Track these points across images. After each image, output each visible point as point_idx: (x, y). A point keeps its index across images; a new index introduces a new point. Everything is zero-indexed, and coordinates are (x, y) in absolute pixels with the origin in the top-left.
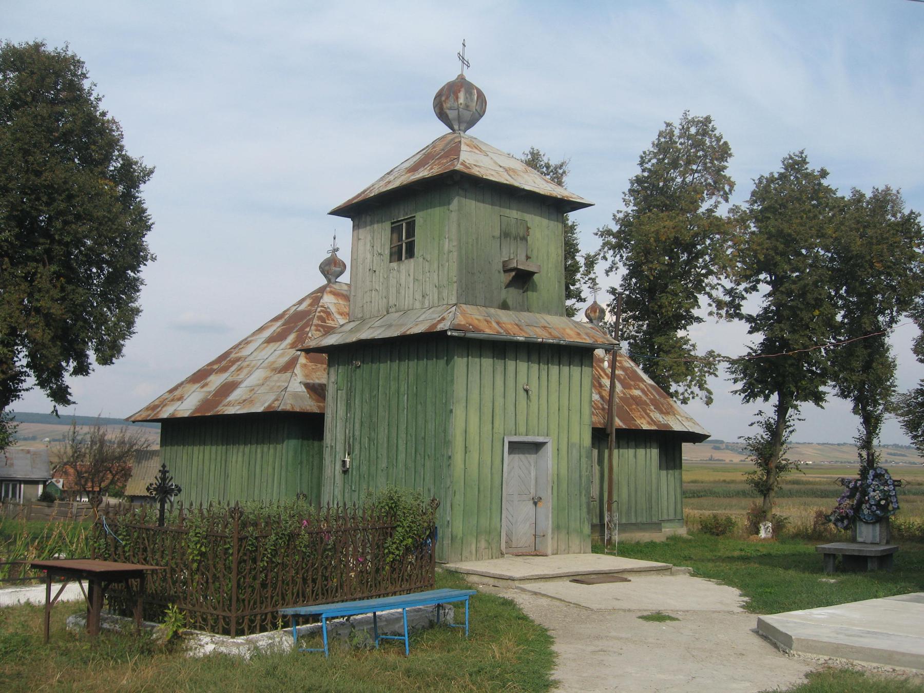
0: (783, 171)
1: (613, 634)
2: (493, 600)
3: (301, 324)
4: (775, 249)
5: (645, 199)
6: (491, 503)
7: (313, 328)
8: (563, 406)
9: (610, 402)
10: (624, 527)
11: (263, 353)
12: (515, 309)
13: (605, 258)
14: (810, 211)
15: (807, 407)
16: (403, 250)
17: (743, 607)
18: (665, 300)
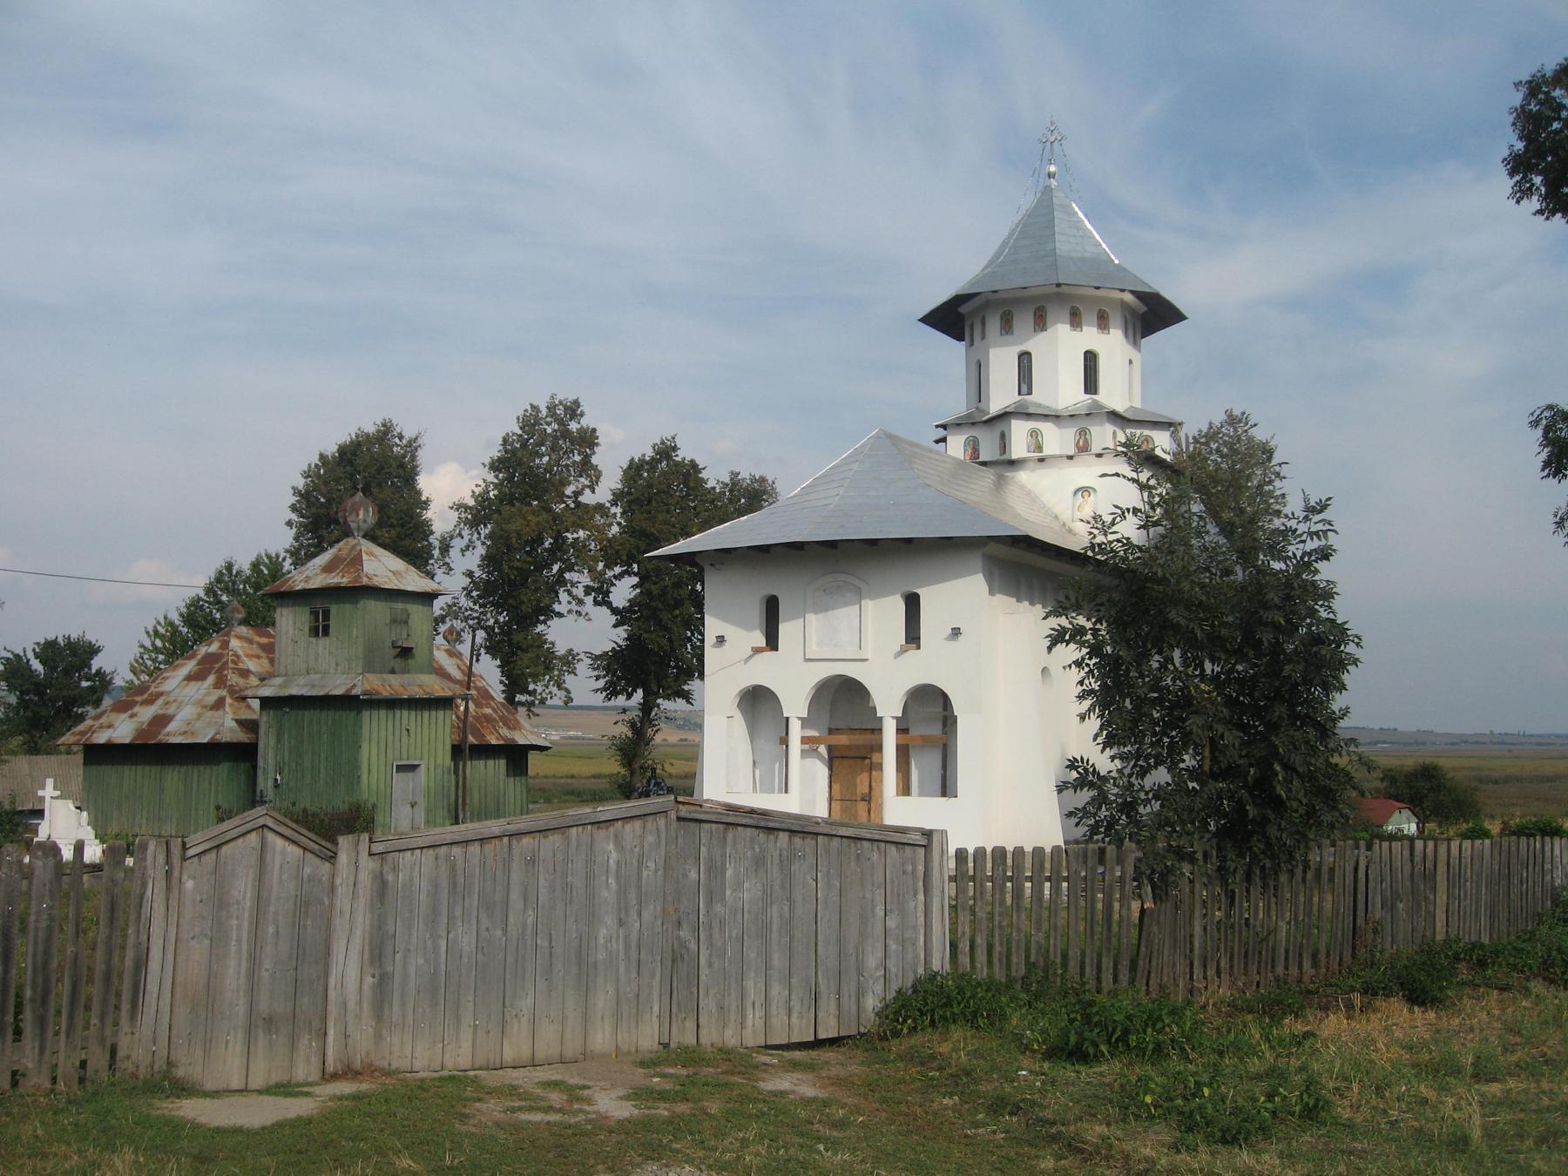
4: (637, 548)
8: (431, 738)
9: (465, 721)
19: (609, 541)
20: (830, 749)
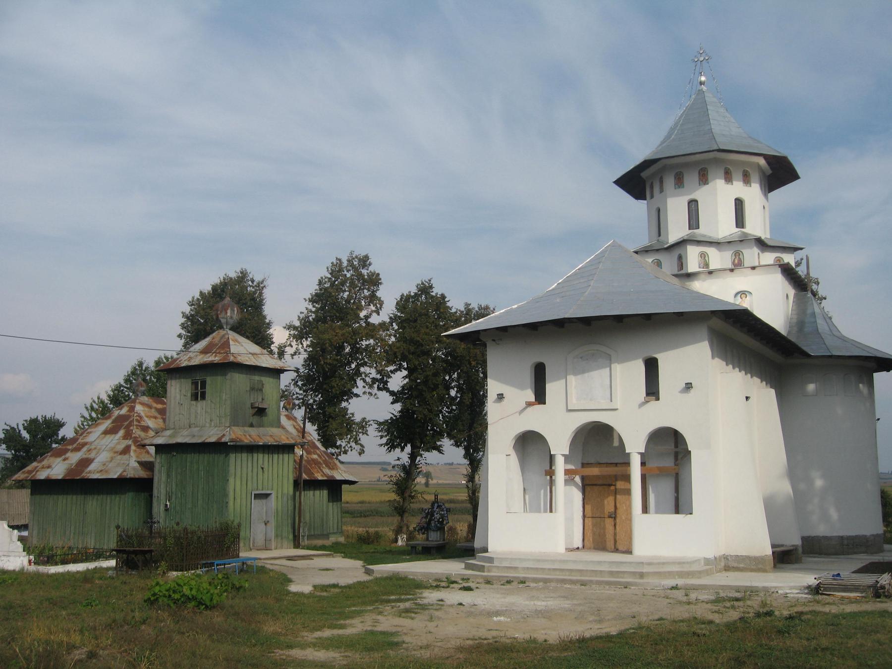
3: (126, 423)
8: (278, 474)
10: (310, 537)
11: (104, 441)
19: (390, 346)
20: (583, 478)
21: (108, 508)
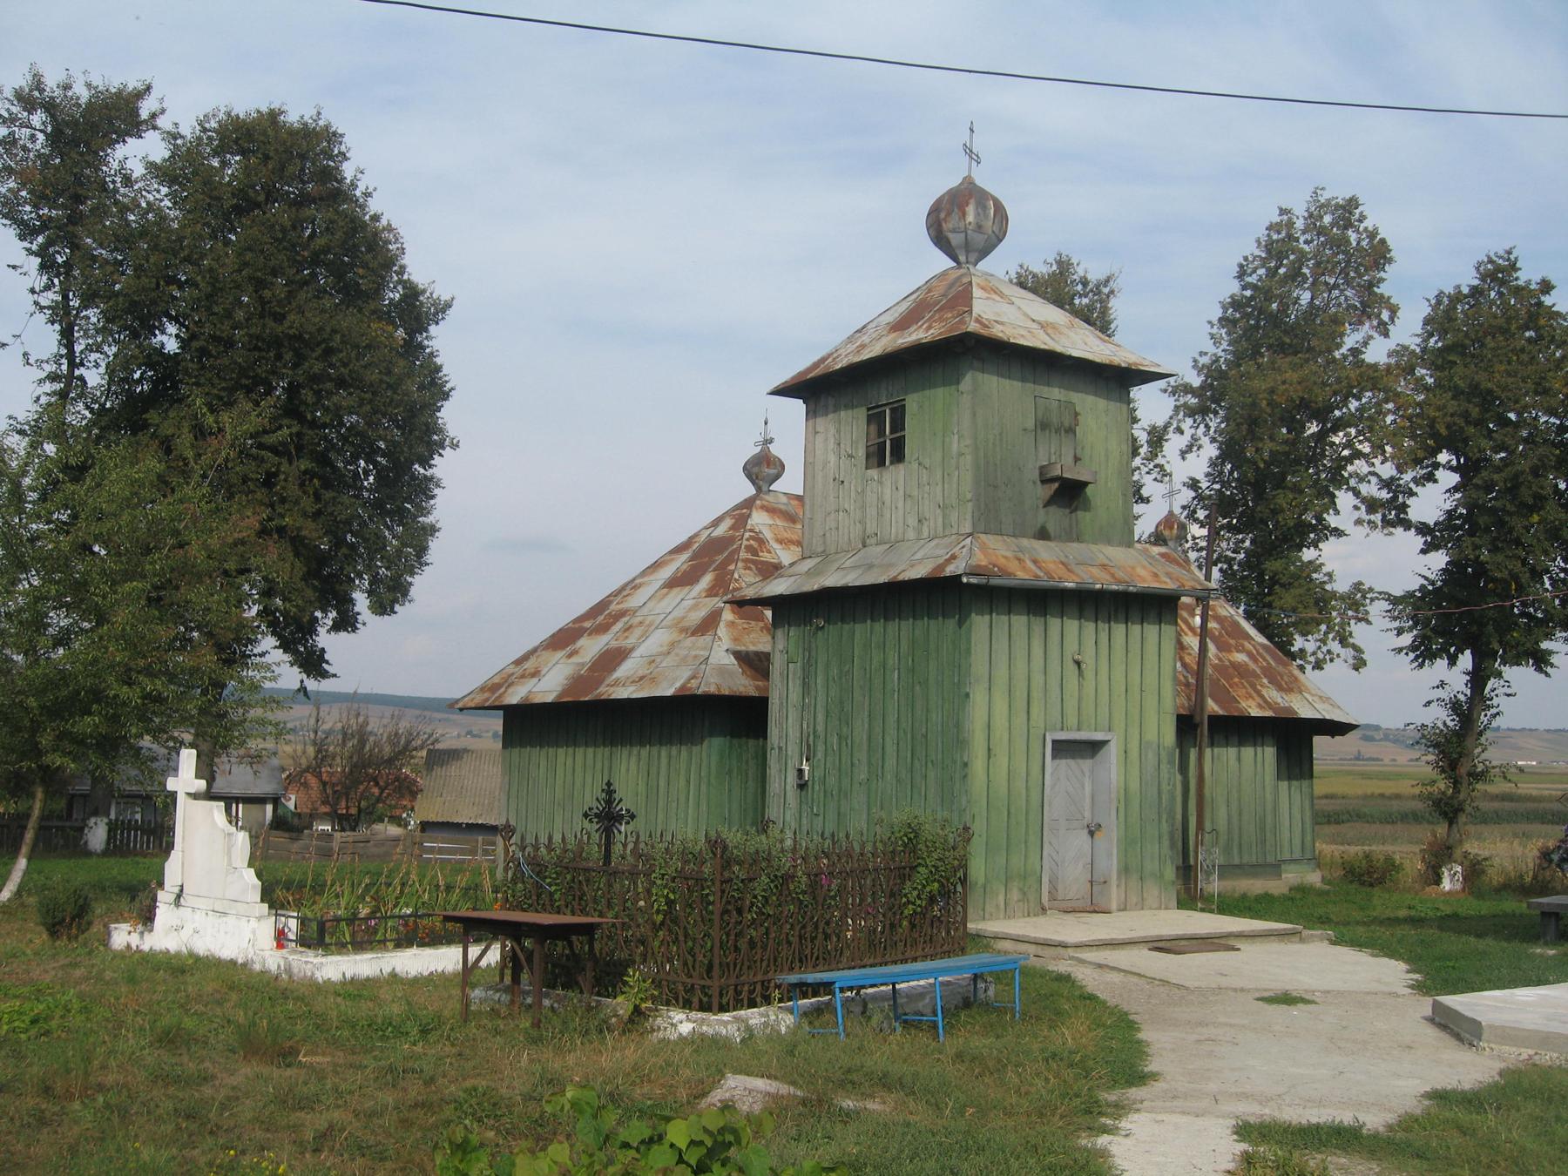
0: (1476, 282)
1: (1222, 1019)
2: (1044, 974)
3: (720, 558)
4: (1466, 415)
5: (1249, 332)
6: (1027, 833)
7: (740, 564)
8: (1129, 685)
9: (1199, 674)
10: (1227, 871)
12: (1058, 538)
13: (1180, 431)
14: (1523, 350)
15: (1519, 676)
16: (887, 450)
17: (1412, 987)
18: (1282, 499)
21: (662, 783)
